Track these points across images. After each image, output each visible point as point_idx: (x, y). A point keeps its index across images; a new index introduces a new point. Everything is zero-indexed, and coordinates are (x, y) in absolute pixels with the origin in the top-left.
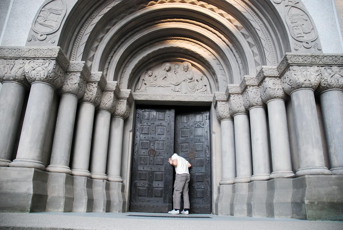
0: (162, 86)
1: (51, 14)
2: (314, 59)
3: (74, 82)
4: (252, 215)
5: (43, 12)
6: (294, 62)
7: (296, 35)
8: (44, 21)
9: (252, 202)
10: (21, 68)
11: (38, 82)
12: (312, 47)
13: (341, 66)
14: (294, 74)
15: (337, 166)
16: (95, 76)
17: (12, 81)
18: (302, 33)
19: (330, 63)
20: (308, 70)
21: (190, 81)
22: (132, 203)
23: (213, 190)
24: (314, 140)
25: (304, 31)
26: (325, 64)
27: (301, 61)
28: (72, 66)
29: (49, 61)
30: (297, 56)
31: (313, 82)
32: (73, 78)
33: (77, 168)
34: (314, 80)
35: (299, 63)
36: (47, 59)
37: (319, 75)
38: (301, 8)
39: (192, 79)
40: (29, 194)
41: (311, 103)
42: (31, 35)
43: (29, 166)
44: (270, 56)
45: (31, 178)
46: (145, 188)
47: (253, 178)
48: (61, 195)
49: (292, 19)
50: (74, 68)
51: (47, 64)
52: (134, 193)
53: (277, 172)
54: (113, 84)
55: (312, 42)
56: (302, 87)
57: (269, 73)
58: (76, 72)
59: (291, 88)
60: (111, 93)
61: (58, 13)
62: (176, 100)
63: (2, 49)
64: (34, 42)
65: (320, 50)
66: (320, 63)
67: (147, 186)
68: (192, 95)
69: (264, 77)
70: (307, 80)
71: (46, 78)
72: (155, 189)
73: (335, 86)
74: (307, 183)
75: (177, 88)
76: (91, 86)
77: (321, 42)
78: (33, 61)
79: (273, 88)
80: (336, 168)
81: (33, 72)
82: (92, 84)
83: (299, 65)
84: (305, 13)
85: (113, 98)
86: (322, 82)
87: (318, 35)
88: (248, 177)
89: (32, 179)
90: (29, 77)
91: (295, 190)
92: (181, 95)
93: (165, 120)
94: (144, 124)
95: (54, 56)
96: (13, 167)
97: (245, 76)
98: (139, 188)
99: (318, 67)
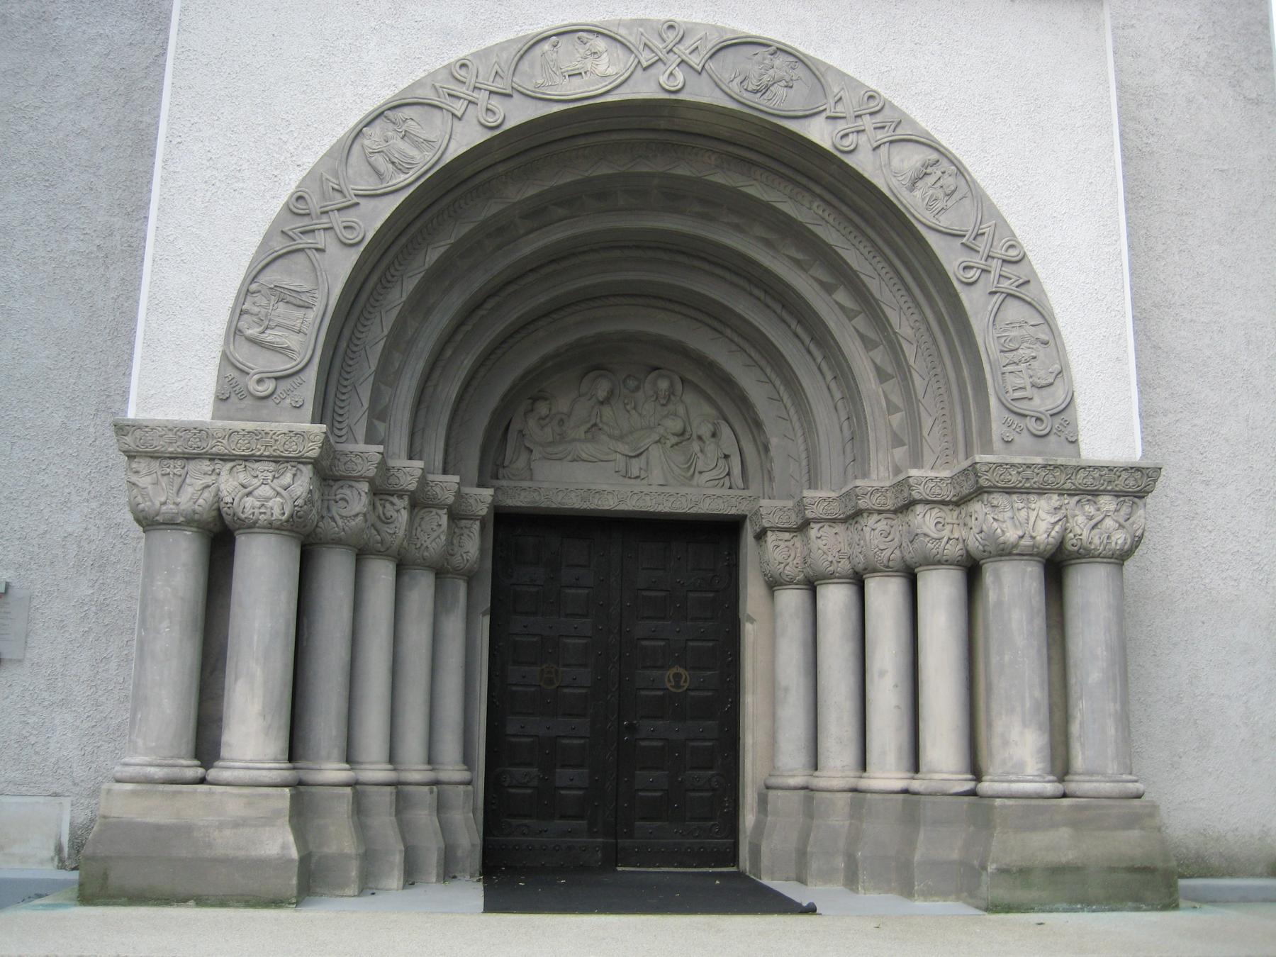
2: (1051, 476)
4: (858, 889)
5: (254, 295)
6: (996, 483)
7: (1011, 391)
8: (261, 329)
9: (859, 854)
12: (1052, 433)
14: (994, 518)
15: (1081, 771)
16: (400, 475)
17: (183, 525)
18: (1028, 387)
19: (1095, 488)
20: (1033, 506)
22: (491, 838)
23: (744, 797)
24: (1028, 705)
25: (1035, 379)
27: (1014, 478)
28: (344, 459)
29: (293, 466)
31: (1041, 541)
32: (346, 497)
34: (1046, 535)
36: (287, 462)
37: (1060, 520)
39: (682, 434)
43: (267, 780)
45: (285, 816)
46: (529, 791)
48: (347, 850)
49: (1004, 339)
50: (350, 465)
51: (288, 478)
52: (494, 807)
53: (929, 776)
54: (445, 484)
56: (1010, 554)
57: (928, 492)
58: (357, 479)
59: (984, 551)
61: (301, 303)
63: (147, 430)
64: (237, 401)
65: (1072, 442)
72: (562, 792)
73: (1100, 553)
78: (243, 466)
79: (935, 536)
80: (1077, 778)
81: (249, 501)
83: (1009, 491)
85: (446, 531)
86: (1067, 539)
87: (1073, 392)
90: (234, 515)
92: (646, 490)
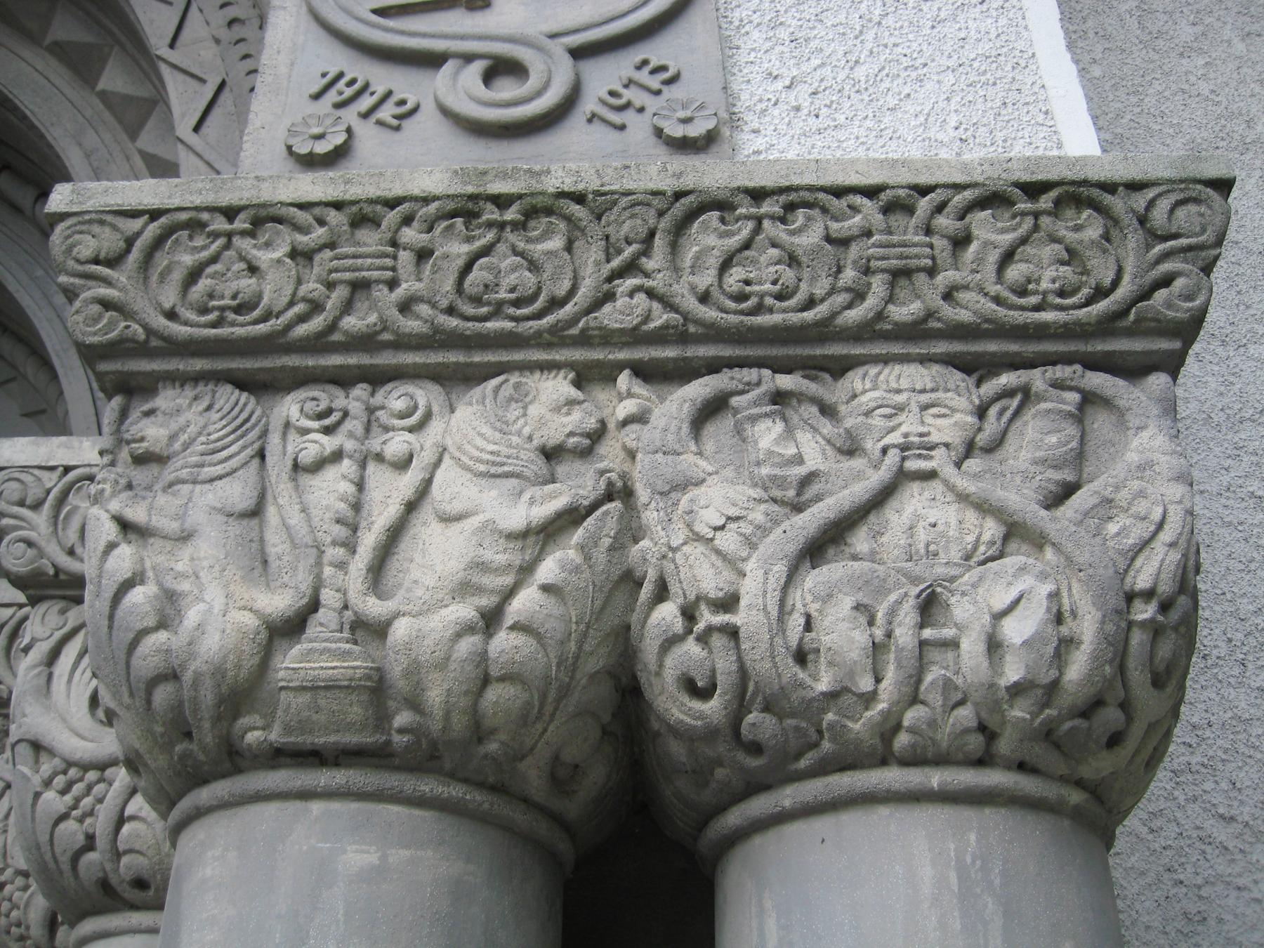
6: (160, 322)
13: (727, 351)
26: (715, 333)
30: (220, 224)
31: (426, 651)
35: (241, 329)
55: (178, 44)
66: (612, 316)
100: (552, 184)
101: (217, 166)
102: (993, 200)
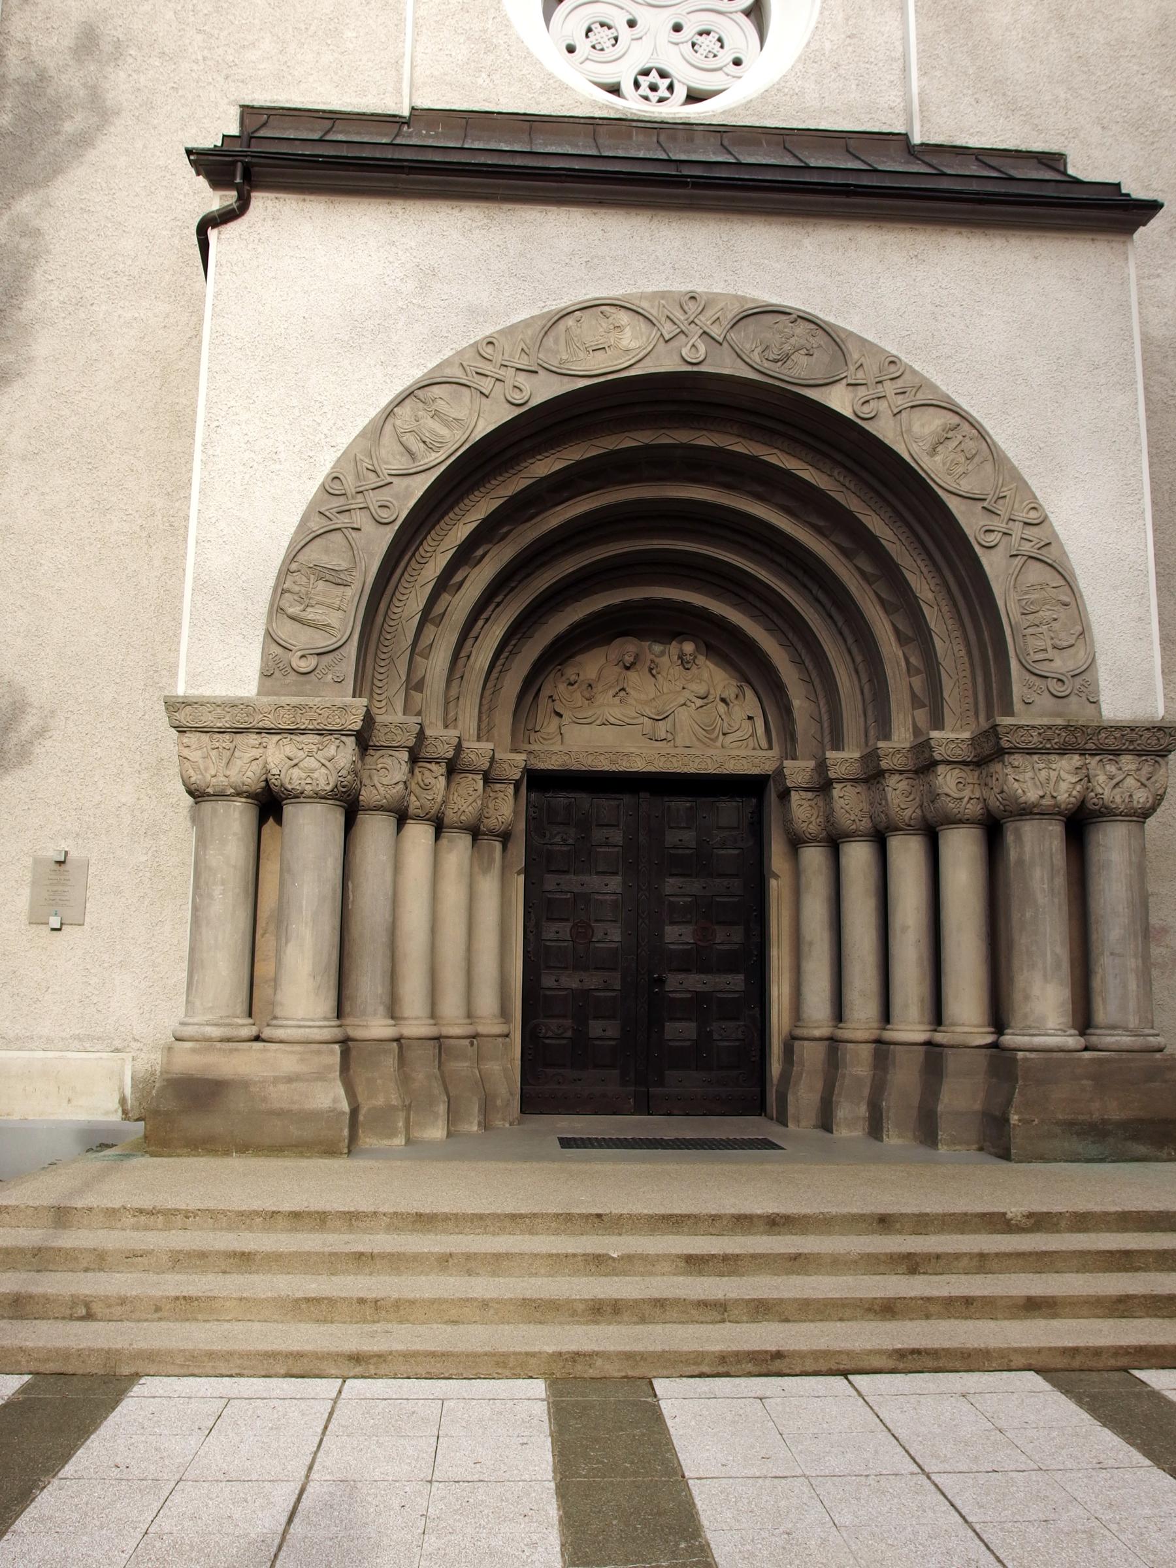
0: (612, 720)
1: (320, 582)
3: (391, 779)
7: (1032, 653)
10: (257, 761)
11: (309, 800)
20: (1054, 766)
21: (699, 702)
33: (406, 1016)
34: (1066, 795)
37: (1081, 780)
38: (1055, 564)
40: (339, 1113)
41: (1051, 858)
42: (271, 657)
44: (956, 690)
46: (564, 1042)
47: (889, 1035)
48: (394, 1102)
53: (953, 1028)
54: (480, 751)
56: (1031, 813)
60: (474, 776)
61: (340, 581)
62: (658, 770)
63: (196, 706)
64: (281, 676)
65: (1094, 703)
66: (1087, 747)
67: (569, 1034)
68: (711, 752)
69: (934, 764)
70: (1048, 798)
71: (332, 791)
74: (1020, 1073)
75: (662, 729)
76: (427, 773)
77: (1100, 674)
80: (1098, 1031)
81: (296, 772)
82: (428, 765)
83: (1030, 752)
84: (1065, 579)
88: (875, 1025)
89: (338, 1073)
91: (994, 1080)
92: (673, 751)
93: (618, 826)
94: (555, 840)
95: (350, 727)
96: (281, 1042)
97: (881, 744)
98: (547, 1041)
99: (1083, 757)
100: (1080, 723)
101: (738, 75)
102: (1148, 729)
